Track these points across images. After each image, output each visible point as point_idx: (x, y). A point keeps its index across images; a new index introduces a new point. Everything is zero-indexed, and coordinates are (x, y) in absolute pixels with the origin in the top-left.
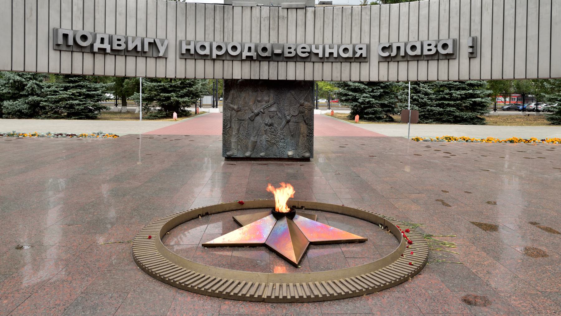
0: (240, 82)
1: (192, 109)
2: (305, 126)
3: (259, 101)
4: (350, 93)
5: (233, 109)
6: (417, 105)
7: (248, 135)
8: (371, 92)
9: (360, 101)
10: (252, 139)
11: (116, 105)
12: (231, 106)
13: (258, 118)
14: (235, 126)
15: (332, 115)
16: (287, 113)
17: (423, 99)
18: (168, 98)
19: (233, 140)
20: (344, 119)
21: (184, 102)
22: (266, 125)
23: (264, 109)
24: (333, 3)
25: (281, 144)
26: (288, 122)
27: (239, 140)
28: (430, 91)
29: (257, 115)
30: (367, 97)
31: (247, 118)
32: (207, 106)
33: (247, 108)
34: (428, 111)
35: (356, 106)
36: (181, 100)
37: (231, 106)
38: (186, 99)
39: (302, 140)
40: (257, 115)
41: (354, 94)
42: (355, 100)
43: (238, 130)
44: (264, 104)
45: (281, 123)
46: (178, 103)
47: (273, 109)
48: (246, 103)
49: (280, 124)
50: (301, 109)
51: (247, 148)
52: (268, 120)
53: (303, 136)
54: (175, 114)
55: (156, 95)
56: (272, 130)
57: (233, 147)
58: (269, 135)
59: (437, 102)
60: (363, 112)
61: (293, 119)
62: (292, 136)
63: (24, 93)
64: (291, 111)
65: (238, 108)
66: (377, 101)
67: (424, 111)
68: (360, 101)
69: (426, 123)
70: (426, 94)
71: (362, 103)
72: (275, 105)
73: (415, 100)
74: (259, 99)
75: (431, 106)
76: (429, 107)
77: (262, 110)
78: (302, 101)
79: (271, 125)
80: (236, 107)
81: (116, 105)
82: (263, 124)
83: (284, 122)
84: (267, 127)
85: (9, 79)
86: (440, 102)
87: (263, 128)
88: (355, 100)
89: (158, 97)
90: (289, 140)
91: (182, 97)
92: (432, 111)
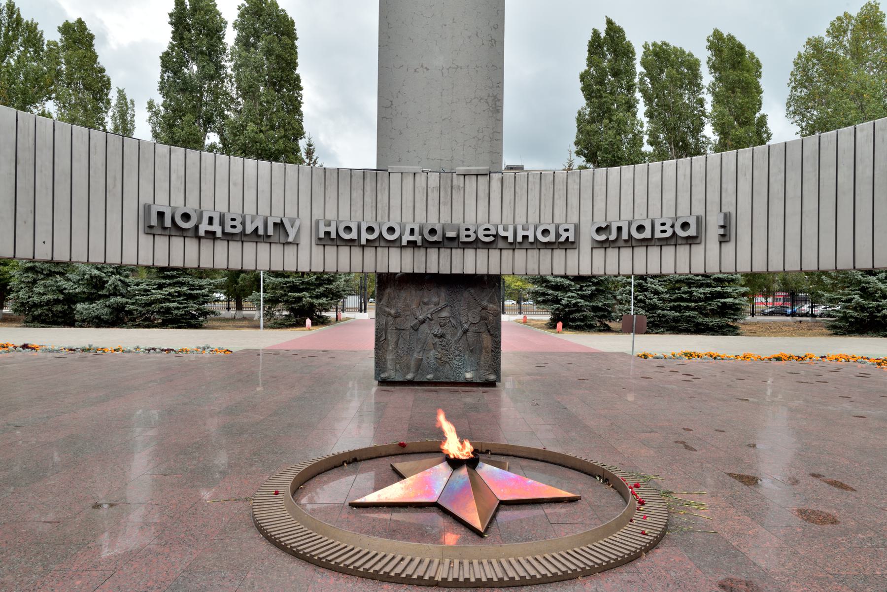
1: (331, 315)
2: (489, 337)
3: (425, 304)
4: (550, 292)
5: (389, 314)
6: (643, 308)
7: (410, 351)
9: (563, 302)
10: (415, 355)
11: (229, 309)
12: (387, 309)
13: (424, 327)
14: (392, 337)
15: (525, 321)
16: (464, 320)
17: (651, 299)
18: (299, 299)
19: (390, 357)
20: (541, 328)
22: (436, 336)
23: (432, 315)
25: (456, 362)
26: (465, 332)
27: (398, 357)
28: (661, 289)
29: (423, 322)
30: (573, 297)
31: (409, 326)
32: (352, 310)
33: (409, 313)
35: (558, 309)
37: (387, 309)
38: (323, 300)
39: (485, 357)
40: (423, 322)
42: (556, 301)
43: (397, 343)
44: (432, 308)
45: (456, 334)
46: (312, 305)
47: (444, 314)
48: (407, 306)
49: (454, 334)
50: (484, 313)
51: (409, 368)
52: (437, 330)
53: (487, 352)
55: (282, 296)
56: (444, 343)
57: (389, 366)
58: (439, 350)
59: (672, 304)
61: (473, 329)
62: (471, 351)
64: (469, 317)
65: (396, 313)
67: (653, 317)
68: (563, 302)
69: (657, 333)
70: (656, 292)
71: (566, 306)
72: (448, 309)
73: (640, 301)
74: (426, 300)
75: (663, 310)
76: (660, 311)
77: (429, 316)
78: (485, 303)
79: (442, 336)
80: (393, 312)
81: (229, 309)
82: (431, 335)
83: (460, 332)
84: (437, 340)
86: (676, 304)
87: (431, 340)
88: (556, 301)
89: (285, 298)
90: (466, 356)
92: (664, 316)
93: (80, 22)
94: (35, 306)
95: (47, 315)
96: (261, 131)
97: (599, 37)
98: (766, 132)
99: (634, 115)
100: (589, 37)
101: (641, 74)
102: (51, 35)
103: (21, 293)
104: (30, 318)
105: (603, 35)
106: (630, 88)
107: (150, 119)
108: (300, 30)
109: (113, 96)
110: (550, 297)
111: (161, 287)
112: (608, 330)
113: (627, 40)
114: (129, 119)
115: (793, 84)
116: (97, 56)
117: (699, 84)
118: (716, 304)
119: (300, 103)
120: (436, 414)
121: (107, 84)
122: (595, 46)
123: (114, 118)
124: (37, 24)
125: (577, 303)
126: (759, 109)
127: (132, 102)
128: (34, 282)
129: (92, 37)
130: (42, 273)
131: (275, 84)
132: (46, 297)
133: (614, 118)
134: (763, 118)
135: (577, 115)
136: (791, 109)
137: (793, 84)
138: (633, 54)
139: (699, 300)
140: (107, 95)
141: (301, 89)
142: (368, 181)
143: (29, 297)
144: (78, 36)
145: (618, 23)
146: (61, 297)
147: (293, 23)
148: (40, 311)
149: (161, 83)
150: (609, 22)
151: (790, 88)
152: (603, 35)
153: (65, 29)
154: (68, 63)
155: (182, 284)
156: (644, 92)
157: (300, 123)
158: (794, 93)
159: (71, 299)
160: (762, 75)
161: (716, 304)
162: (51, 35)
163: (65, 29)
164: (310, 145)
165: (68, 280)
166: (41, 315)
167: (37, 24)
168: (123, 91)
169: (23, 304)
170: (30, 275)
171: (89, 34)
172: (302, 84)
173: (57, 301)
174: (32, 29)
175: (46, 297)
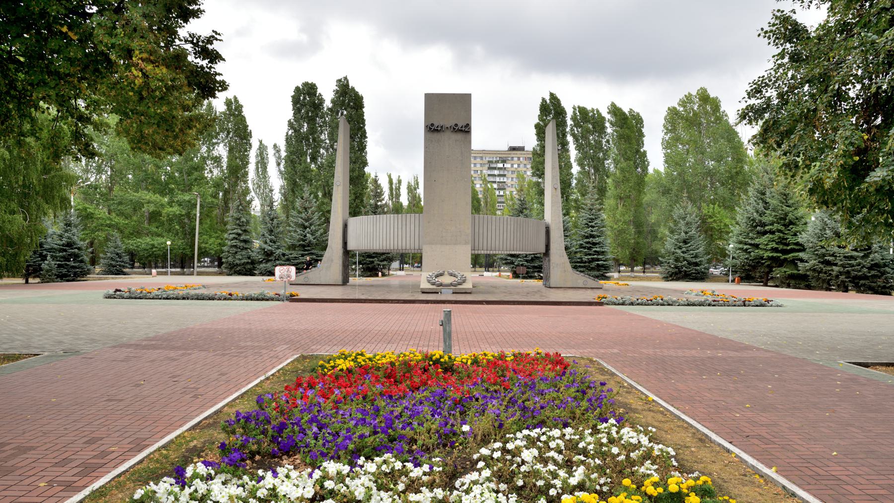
18: (373, 262)
42: (512, 263)
54: (380, 274)
91: (381, 261)
94: (237, 265)
103: (230, 259)
104: (232, 271)
105: (548, 101)
108: (366, 102)
109: (255, 142)
111: (303, 255)
112: (830, 290)
118: (594, 264)
120: (409, 206)
121: (250, 135)
122: (545, 109)
123: (257, 156)
129: (242, 106)
139: (585, 262)
147: (362, 98)
150: (552, 95)
152: (548, 101)
155: (312, 254)
156: (573, 135)
161: (594, 264)
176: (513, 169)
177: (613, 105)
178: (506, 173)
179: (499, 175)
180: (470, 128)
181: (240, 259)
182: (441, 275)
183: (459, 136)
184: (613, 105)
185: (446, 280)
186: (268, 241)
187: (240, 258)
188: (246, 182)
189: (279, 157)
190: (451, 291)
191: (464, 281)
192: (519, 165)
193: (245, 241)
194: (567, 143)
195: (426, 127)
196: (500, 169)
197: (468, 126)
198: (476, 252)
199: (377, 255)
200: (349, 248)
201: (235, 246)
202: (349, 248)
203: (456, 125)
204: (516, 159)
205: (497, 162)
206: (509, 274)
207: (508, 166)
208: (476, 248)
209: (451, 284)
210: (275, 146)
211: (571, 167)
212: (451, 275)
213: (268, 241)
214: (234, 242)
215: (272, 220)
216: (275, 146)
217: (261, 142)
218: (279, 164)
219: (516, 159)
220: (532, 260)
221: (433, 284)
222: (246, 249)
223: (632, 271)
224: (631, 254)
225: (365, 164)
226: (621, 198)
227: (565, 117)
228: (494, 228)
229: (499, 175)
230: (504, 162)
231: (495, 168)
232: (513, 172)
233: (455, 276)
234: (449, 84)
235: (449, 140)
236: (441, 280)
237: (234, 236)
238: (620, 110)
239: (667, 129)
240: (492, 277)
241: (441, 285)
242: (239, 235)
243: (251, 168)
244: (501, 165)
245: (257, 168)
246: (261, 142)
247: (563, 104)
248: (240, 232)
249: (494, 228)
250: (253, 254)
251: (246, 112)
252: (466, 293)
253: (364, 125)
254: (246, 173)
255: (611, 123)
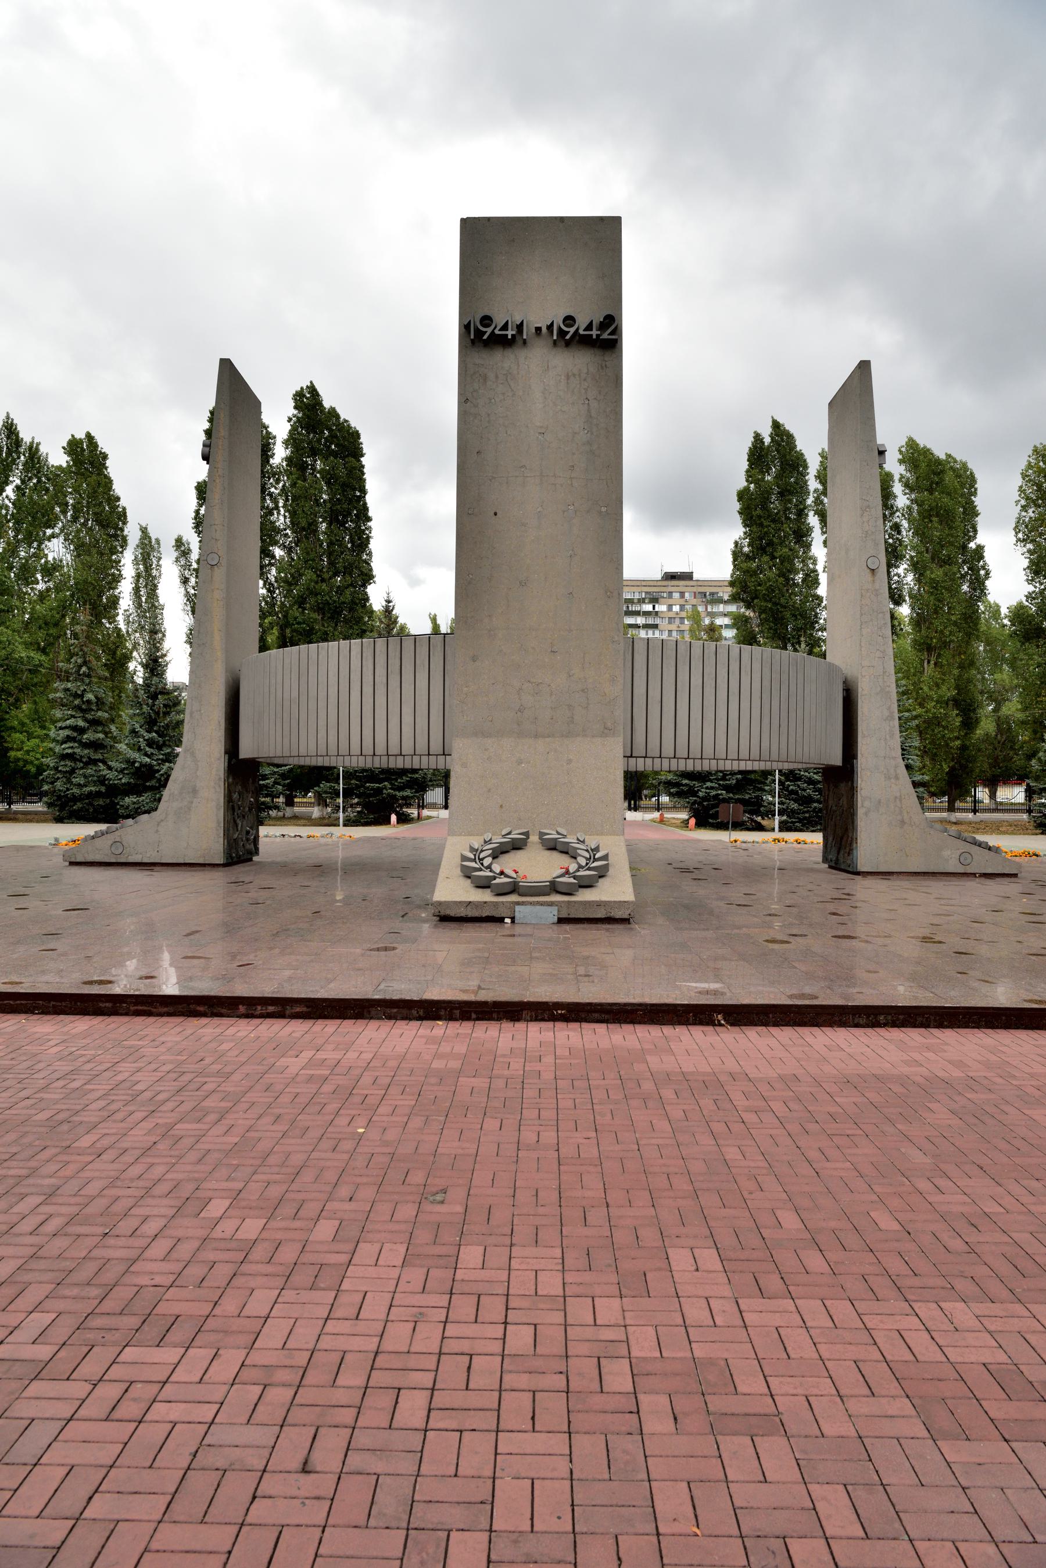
0: (75, 464)
1: (414, 812)
4: (685, 782)
6: (795, 801)
8: (721, 780)
9: (701, 794)
15: (662, 821)
17: (805, 790)
18: (379, 791)
20: (677, 827)
21: (404, 798)
24: (695, 577)
30: (712, 788)
32: (433, 806)
34: (814, 810)
35: (695, 802)
36: (399, 794)
38: (407, 793)
41: (692, 783)
42: (692, 792)
46: (394, 797)
54: (394, 818)
55: (358, 787)
60: (706, 817)
63: (153, 783)
66: (731, 795)
67: (807, 812)
68: (701, 794)
71: (704, 799)
73: (792, 792)
76: (815, 805)
85: (134, 762)
88: (692, 792)
89: (362, 790)
91: (400, 789)
93: (89, 437)
94: (75, 799)
95: (87, 810)
96: (323, 580)
97: (763, 443)
98: (983, 568)
99: (808, 546)
100: (748, 442)
101: (816, 491)
102: (57, 458)
103: (58, 784)
104: (65, 813)
105: (767, 440)
106: (801, 513)
107: (177, 560)
109: (132, 533)
110: (685, 789)
113: (798, 449)
114: (155, 562)
115: (1023, 502)
116: (111, 482)
117: (892, 506)
119: (368, 538)
121: (123, 516)
122: (758, 456)
123: (136, 561)
124: (38, 444)
125: (718, 795)
126: (975, 537)
127: (158, 541)
128: (73, 771)
130: (81, 761)
131: (336, 518)
132: (88, 789)
133: (777, 554)
134: (980, 549)
135: (732, 546)
136: (1020, 535)
137: (1023, 502)
138: (806, 467)
140: (122, 530)
141: (369, 519)
142: (905, 1270)
143: (68, 790)
144: (87, 456)
145: (789, 426)
146: (103, 789)
147: (357, 435)
148: (79, 805)
149: (195, 518)
150: (776, 425)
151: (1019, 507)
152: (767, 440)
153: (73, 447)
154: (76, 490)
157: (369, 564)
158: (1024, 514)
159: (115, 791)
160: (978, 492)
162: (57, 458)
163: (73, 447)
164: (389, 601)
165: (110, 768)
166: (80, 810)
167: (38, 444)
168: (146, 528)
169: (59, 797)
170: (69, 763)
171: (101, 453)
172: (370, 514)
173: (98, 794)
174: (33, 451)
175: (88, 789)
176: (671, 614)
177: (911, 444)
178: (658, 621)
179: (646, 626)
180: (617, 331)
181: (79, 785)
182: (517, 846)
183: (581, 361)
184: (911, 444)
185: (536, 866)
186: (143, 744)
187: (82, 783)
188: (112, 619)
189: (187, 566)
190: (551, 914)
191: (602, 873)
192: (682, 607)
193: (96, 745)
194: (810, 530)
195: (465, 328)
196: (647, 614)
197: (611, 323)
198: (640, 765)
199: (389, 774)
200: (247, 750)
201: (71, 757)
202: (247, 750)
203: (569, 320)
204: (676, 595)
205: (641, 601)
206: (684, 815)
207: (661, 608)
208: (639, 750)
209: (554, 888)
210: (179, 542)
211: (816, 583)
212: (553, 846)
213: (143, 744)
214: (67, 748)
215: (154, 697)
216: (179, 542)
217: (144, 531)
218: (185, 581)
219: (676, 595)
220: (739, 787)
221: (483, 885)
222: (95, 762)
223: (951, 808)
224: (952, 769)
225: (368, 577)
226: (930, 649)
227: (803, 474)
228: (696, 680)
229: (646, 626)
230: (654, 600)
231: (637, 613)
232: (671, 620)
233: (566, 851)
234: (543, 178)
235: (542, 375)
236: (513, 865)
237: (67, 732)
238: (927, 452)
239: (1027, 498)
240: (642, 824)
241: (514, 888)
242: (81, 731)
243: (125, 589)
244: (648, 607)
245: (137, 590)
246: (144, 531)
247: (800, 445)
248: (81, 723)
249: (696, 680)
250: (111, 775)
251: (114, 469)
252: (609, 920)
253: (364, 492)
254: (114, 602)
255: (907, 485)
